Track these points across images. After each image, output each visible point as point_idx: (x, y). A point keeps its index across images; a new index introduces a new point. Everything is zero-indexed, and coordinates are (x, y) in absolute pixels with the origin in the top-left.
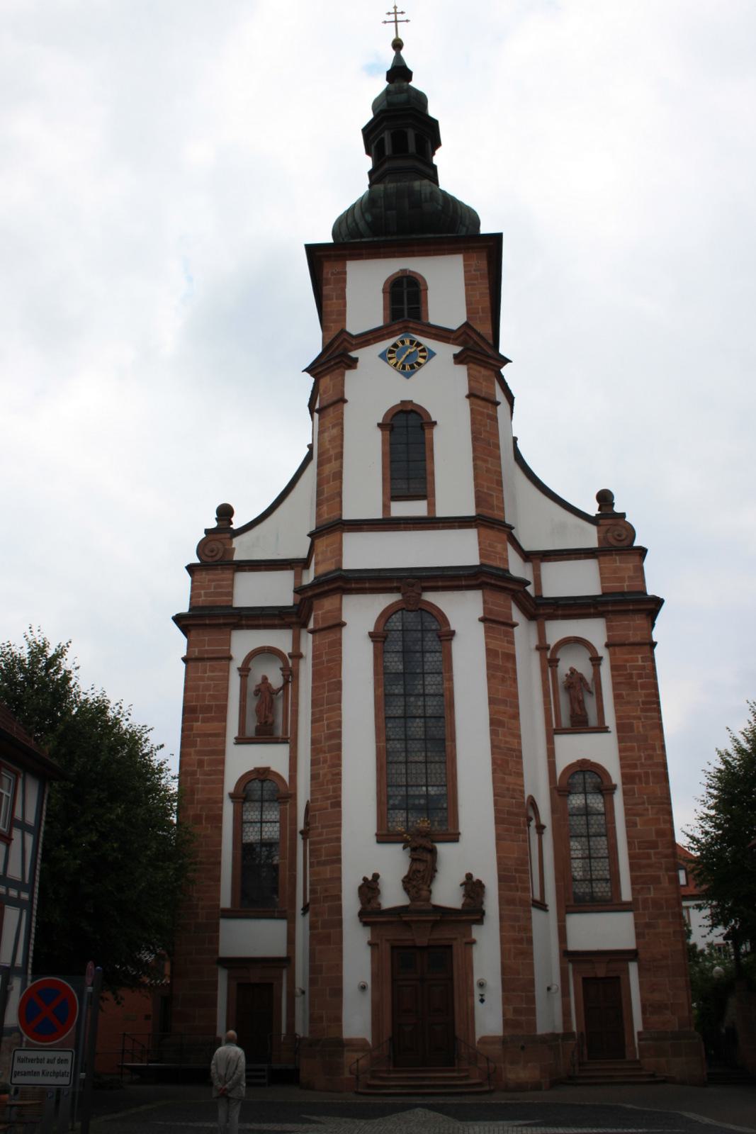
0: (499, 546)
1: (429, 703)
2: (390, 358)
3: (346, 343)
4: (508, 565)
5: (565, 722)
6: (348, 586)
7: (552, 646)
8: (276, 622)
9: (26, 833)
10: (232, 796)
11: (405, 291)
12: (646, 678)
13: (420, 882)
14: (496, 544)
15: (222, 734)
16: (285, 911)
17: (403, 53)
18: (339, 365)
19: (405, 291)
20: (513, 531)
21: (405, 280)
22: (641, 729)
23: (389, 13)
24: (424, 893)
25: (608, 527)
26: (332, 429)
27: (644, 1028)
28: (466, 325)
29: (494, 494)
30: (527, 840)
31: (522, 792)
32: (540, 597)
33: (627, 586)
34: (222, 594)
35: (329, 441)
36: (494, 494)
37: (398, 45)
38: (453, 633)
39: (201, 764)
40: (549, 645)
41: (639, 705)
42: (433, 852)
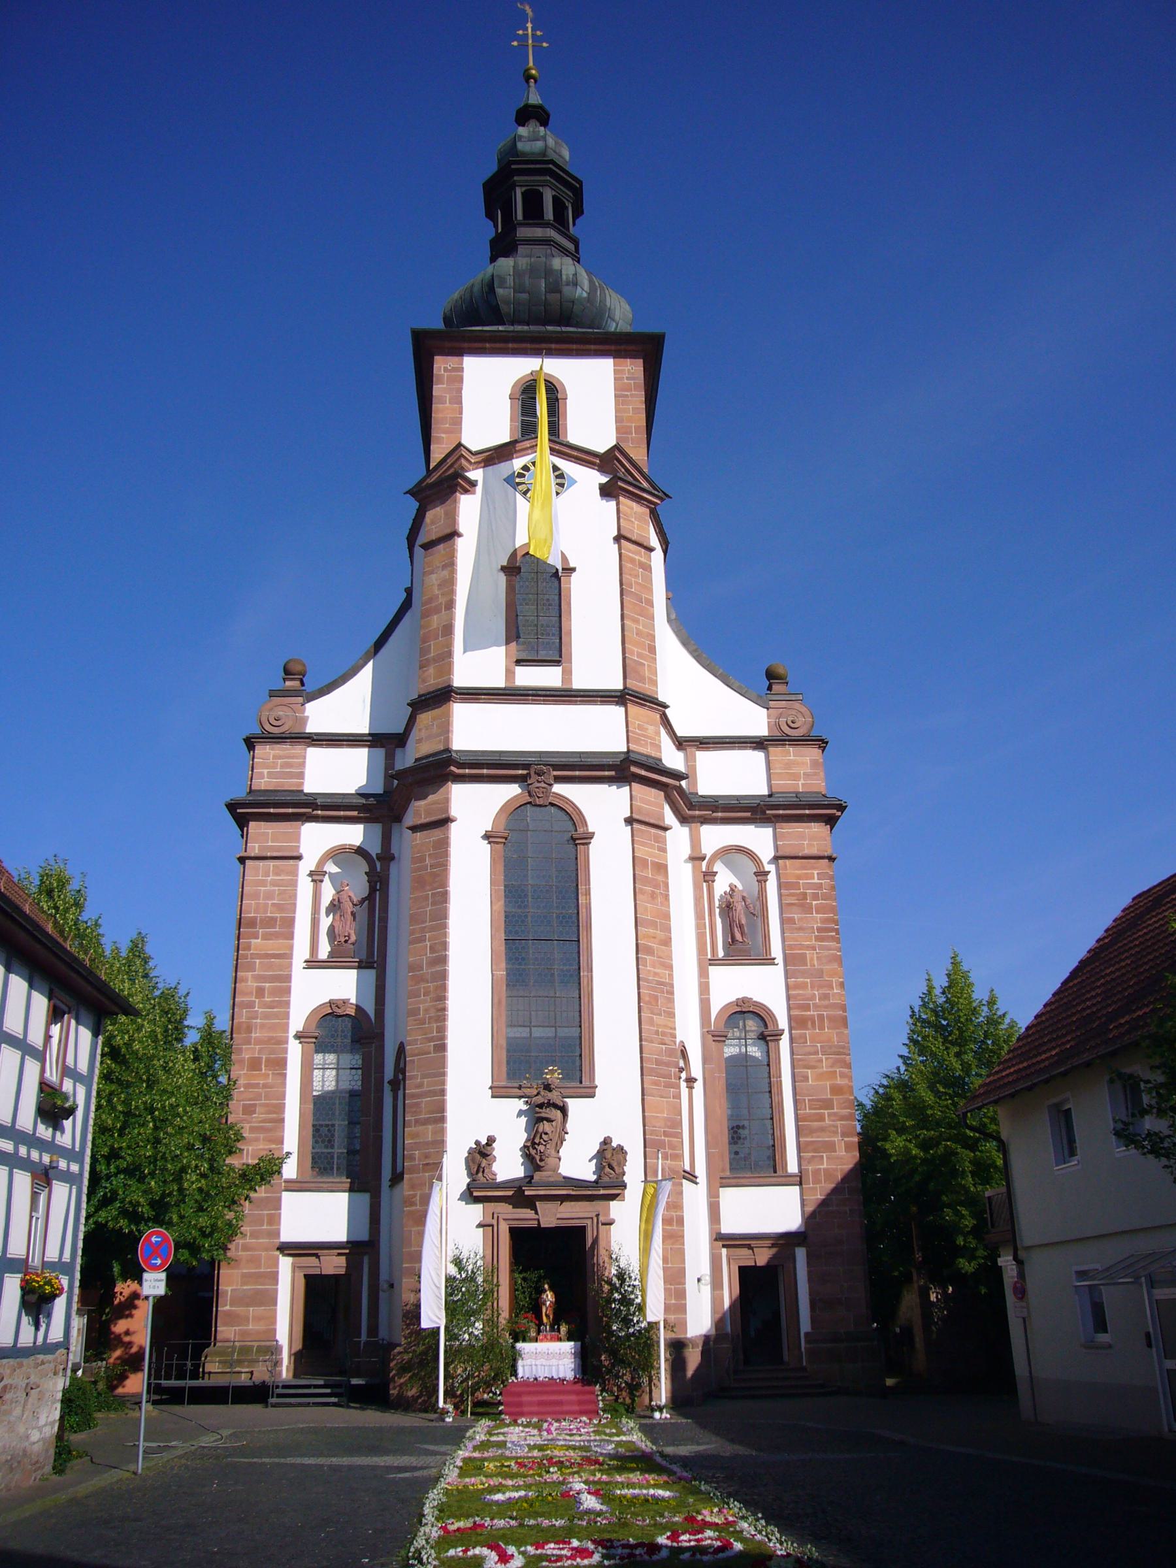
0: (651, 729)
3: (463, 461)
9: (77, 1084)
10: (298, 1036)
12: (822, 900)
14: (646, 726)
15: (288, 956)
20: (667, 711)
22: (816, 963)
26: (443, 570)
28: (616, 447)
29: (646, 663)
30: (678, 1096)
31: (674, 1036)
33: (803, 784)
34: (291, 775)
35: (439, 585)
36: (646, 663)
38: (591, 836)
39: (260, 992)
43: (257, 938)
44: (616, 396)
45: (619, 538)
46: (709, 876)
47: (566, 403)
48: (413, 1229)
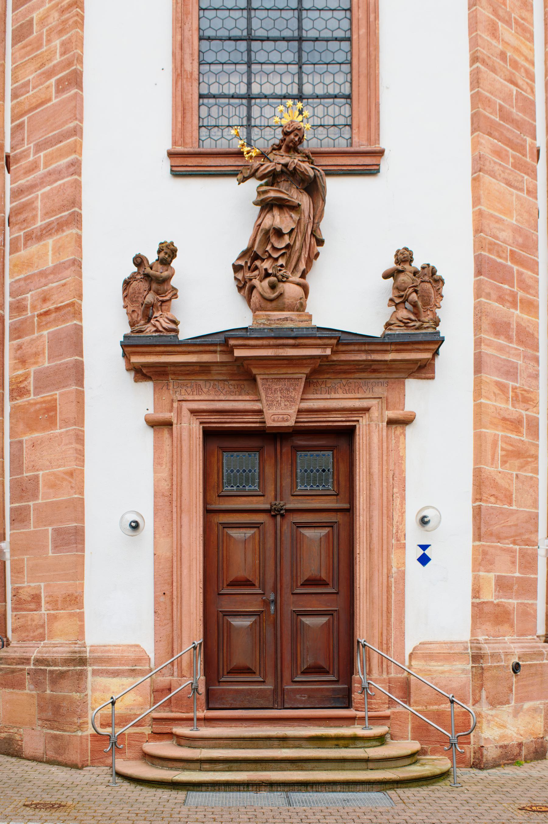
1: (261, 57)
13: (281, 262)
48: (25, 438)
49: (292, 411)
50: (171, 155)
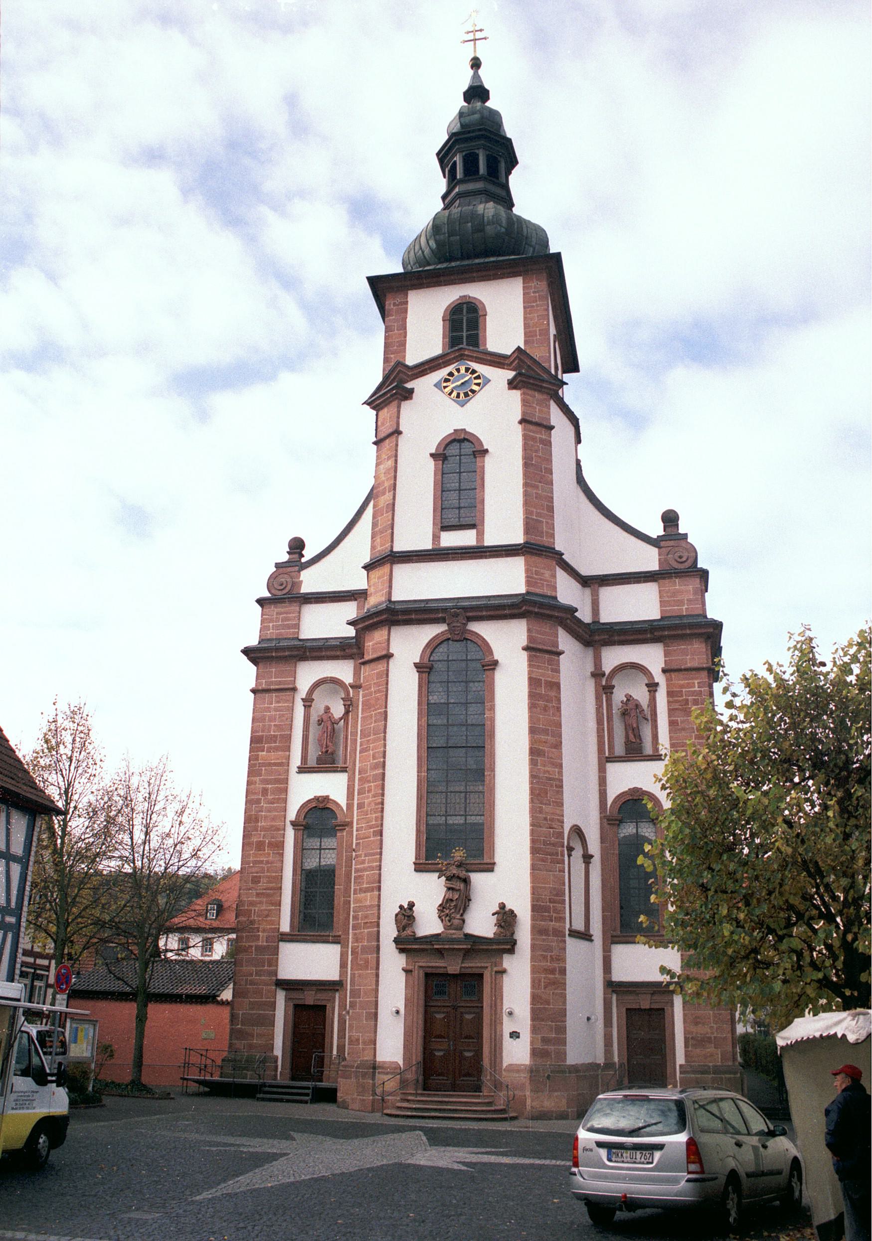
0: (547, 574)
2: (445, 387)
4: (556, 592)
5: (620, 750)
6: (396, 618)
7: (607, 673)
8: (338, 653)
10: (293, 824)
11: (465, 318)
15: (286, 764)
16: (339, 936)
17: (481, 72)
18: (395, 397)
19: (465, 318)
20: (563, 557)
21: (465, 306)
23: (468, 33)
24: (456, 922)
25: (670, 548)
27: (686, 1061)
32: (596, 622)
37: (476, 64)
40: (604, 672)
41: (694, 732)
42: (466, 881)
43: (263, 751)
44: (524, 307)
45: (523, 421)
46: (608, 689)
47: (485, 319)
49: (459, 968)
50: (415, 863)
